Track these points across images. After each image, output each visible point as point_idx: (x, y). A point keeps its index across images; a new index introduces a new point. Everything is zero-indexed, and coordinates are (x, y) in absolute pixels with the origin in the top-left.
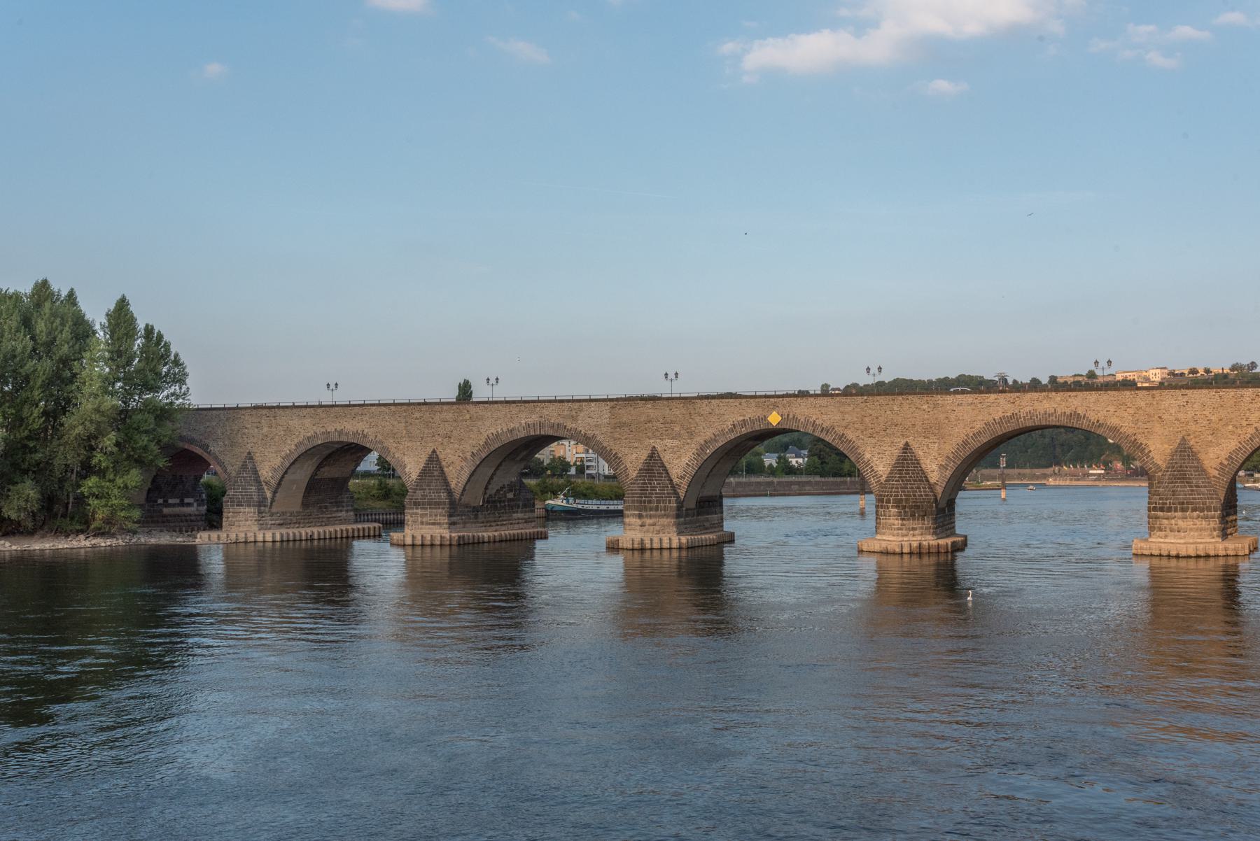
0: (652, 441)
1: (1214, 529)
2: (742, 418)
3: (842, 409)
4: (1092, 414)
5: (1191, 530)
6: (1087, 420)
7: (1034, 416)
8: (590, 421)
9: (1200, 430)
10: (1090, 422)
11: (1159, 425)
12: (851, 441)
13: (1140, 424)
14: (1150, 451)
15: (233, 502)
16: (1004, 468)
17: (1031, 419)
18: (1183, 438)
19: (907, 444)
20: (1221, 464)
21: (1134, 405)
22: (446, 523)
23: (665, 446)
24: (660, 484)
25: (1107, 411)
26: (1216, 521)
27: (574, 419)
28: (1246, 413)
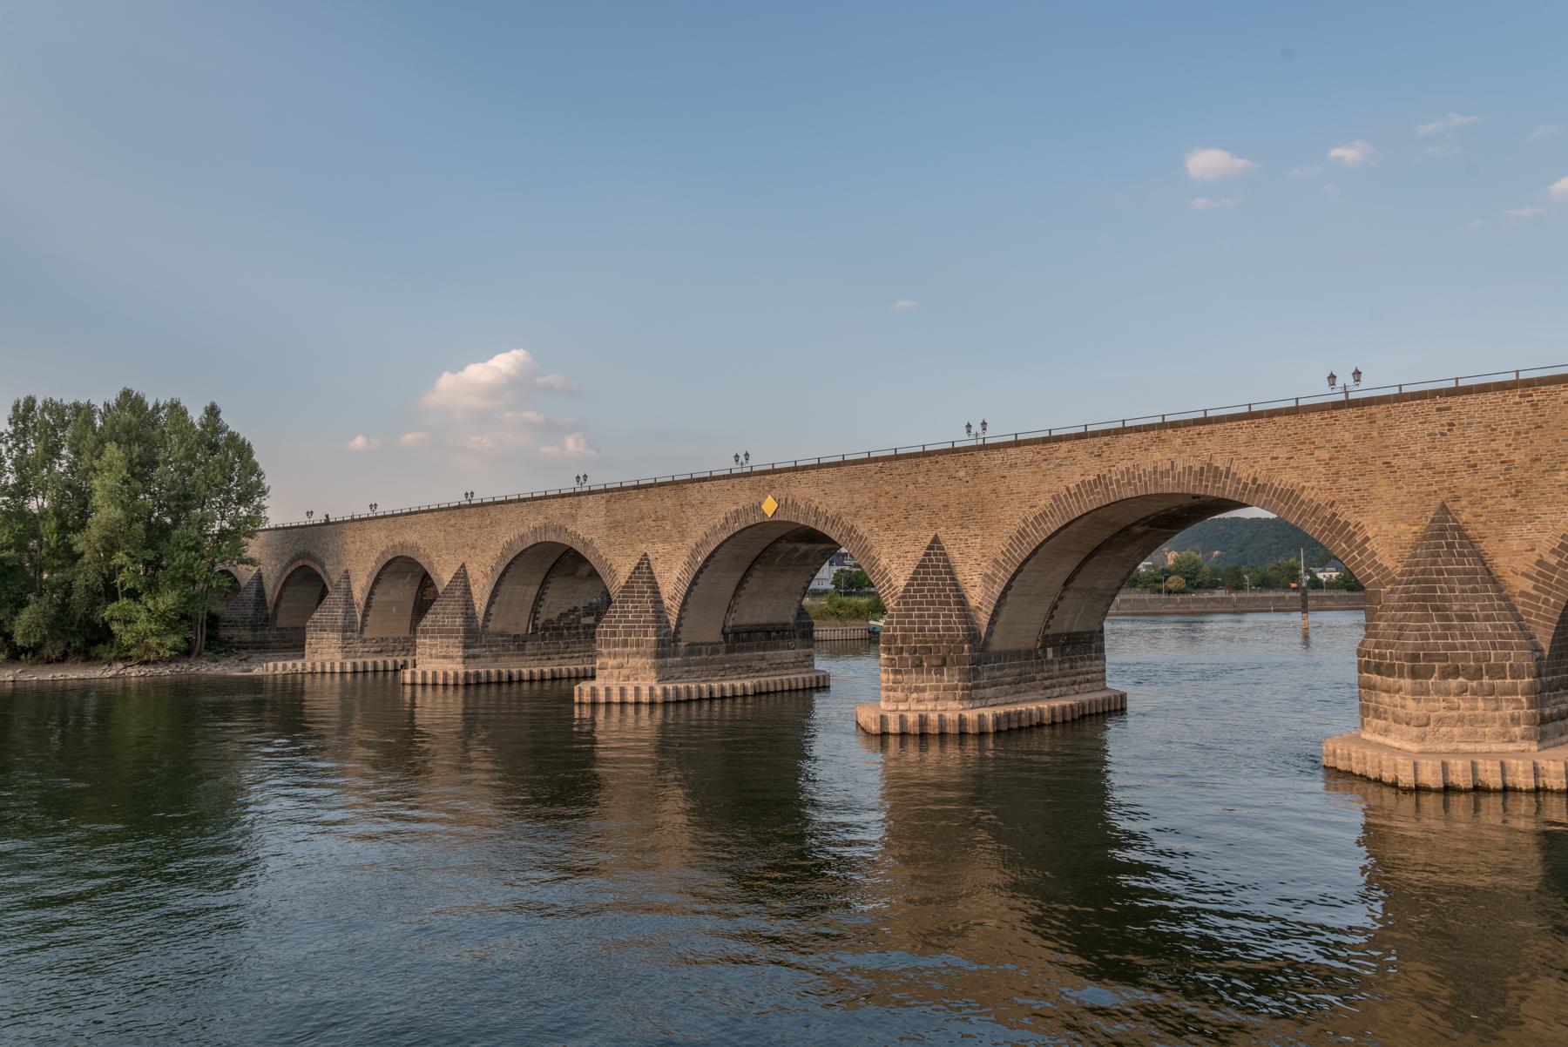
0: (644, 546)
1: (1515, 721)
2: (734, 508)
3: (850, 486)
4: (1243, 466)
5: (1440, 720)
6: (1233, 479)
7: (1134, 478)
8: (588, 521)
9: (1483, 486)
10: (1239, 483)
11: (1386, 482)
12: (862, 537)
13: (1343, 480)
14: (1367, 539)
17: (1129, 483)
18: (1443, 506)
19: (936, 540)
20: (1540, 563)
21: (1327, 441)
22: (461, 657)
23: (656, 549)
24: (637, 607)
25: (1273, 458)
26: (1519, 701)
27: (574, 518)
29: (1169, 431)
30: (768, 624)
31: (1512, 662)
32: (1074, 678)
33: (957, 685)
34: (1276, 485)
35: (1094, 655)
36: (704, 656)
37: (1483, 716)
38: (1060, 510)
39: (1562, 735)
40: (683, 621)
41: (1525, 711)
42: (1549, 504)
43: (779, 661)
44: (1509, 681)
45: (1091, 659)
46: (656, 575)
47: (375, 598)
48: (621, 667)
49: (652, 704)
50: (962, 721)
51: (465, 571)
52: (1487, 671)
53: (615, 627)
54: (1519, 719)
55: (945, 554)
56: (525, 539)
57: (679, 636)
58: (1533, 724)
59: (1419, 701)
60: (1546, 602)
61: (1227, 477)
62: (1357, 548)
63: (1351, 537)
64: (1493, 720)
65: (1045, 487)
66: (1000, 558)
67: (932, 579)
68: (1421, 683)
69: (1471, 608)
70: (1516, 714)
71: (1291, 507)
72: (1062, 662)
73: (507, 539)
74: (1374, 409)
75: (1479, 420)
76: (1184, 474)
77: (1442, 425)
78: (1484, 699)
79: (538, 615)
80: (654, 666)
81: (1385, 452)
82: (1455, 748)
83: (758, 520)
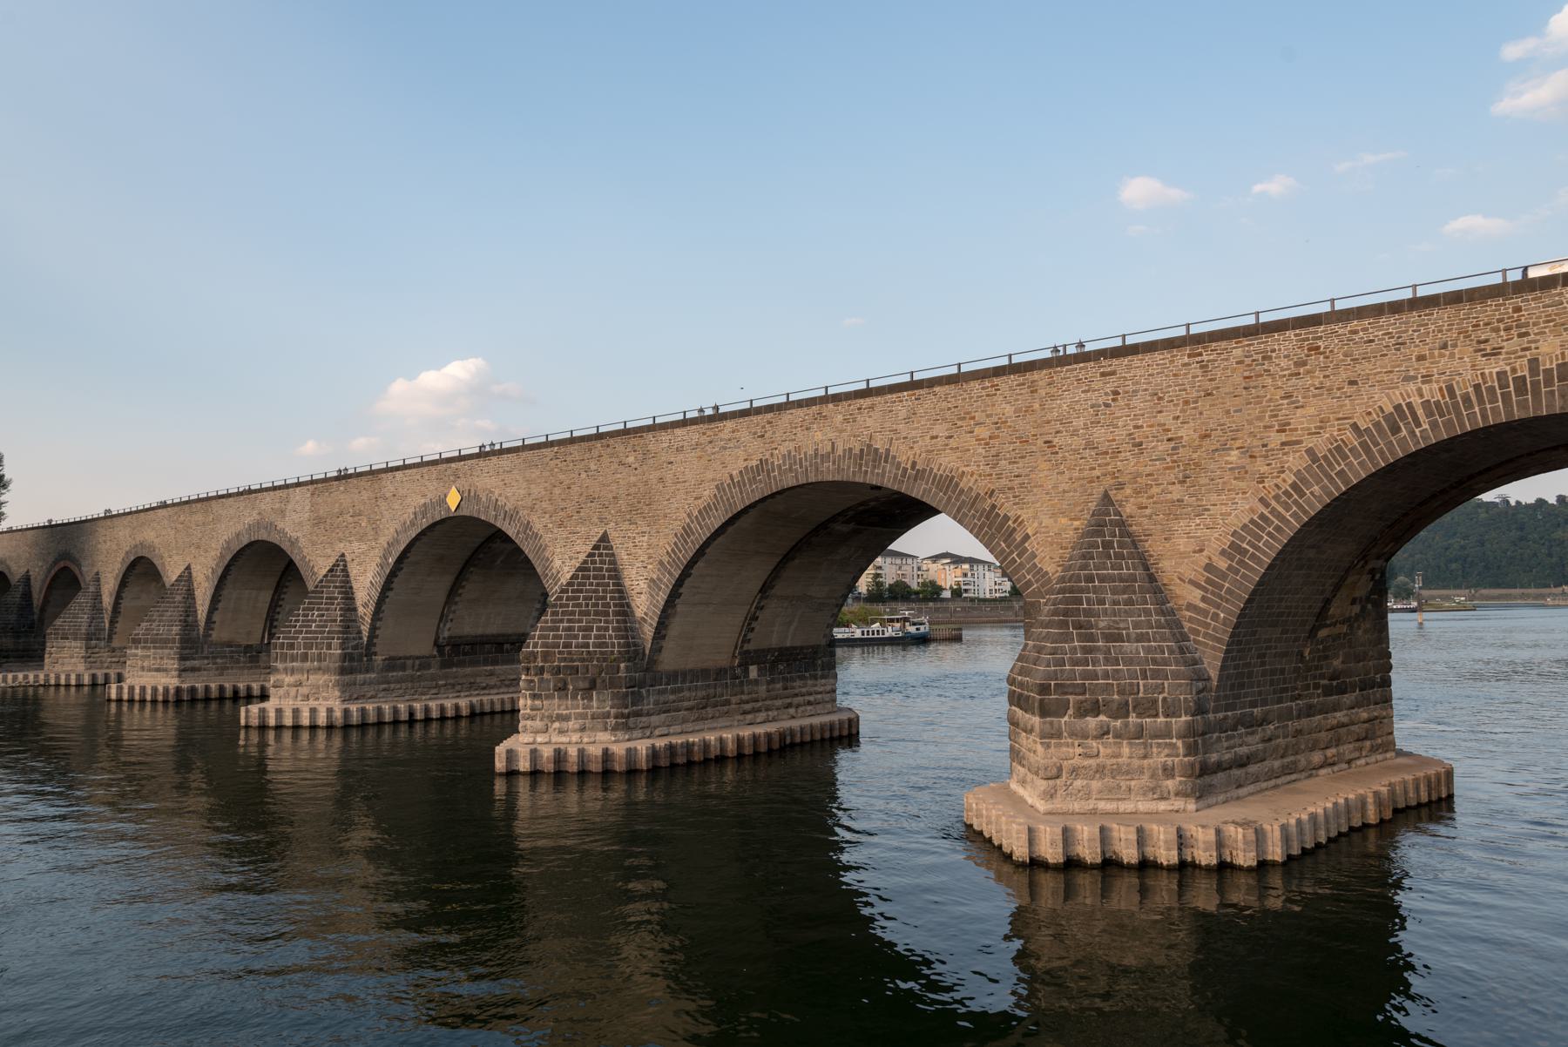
0: (342, 545)
1: (1168, 772)
2: (423, 501)
5: (1075, 771)
8: (295, 516)
9: (1148, 470)
14: (1027, 537)
15: (58, 634)
16: (1420, 588)
18: (1106, 496)
19: (604, 538)
20: (1209, 567)
21: (988, 416)
23: (353, 549)
24: (323, 615)
25: (932, 438)
26: (1174, 746)
28: (1278, 408)
29: (831, 406)
30: (499, 635)
31: (1165, 695)
32: (789, 701)
33: (609, 713)
34: (935, 471)
35: (820, 673)
36: (409, 672)
37: (1129, 765)
38: (723, 501)
39: (1239, 786)
40: (378, 632)
41: (1180, 759)
42: (1219, 492)
43: (512, 677)
44: (1161, 719)
45: (815, 677)
46: (352, 579)
47: (125, 604)
48: (300, 684)
49: (330, 727)
50: (607, 755)
51: (190, 573)
52: (1135, 708)
53: (293, 638)
54: (1173, 769)
55: (613, 555)
56: (241, 537)
57: (373, 649)
58: (1190, 776)
59: (1048, 746)
60: (1215, 616)
61: (886, 462)
62: (1017, 547)
63: (1011, 534)
64: (1141, 771)
65: (709, 475)
66: (666, 559)
67: (591, 584)
68: (1051, 723)
69: (1122, 625)
70: (1170, 763)
71: (950, 498)
72: (772, 681)
73: (226, 537)
74: (1036, 375)
75: (1145, 387)
76: (844, 456)
77: (1106, 394)
78: (1130, 744)
79: (275, 623)
80: (337, 684)
81: (1047, 428)
82: (1091, 807)
83: (444, 515)
